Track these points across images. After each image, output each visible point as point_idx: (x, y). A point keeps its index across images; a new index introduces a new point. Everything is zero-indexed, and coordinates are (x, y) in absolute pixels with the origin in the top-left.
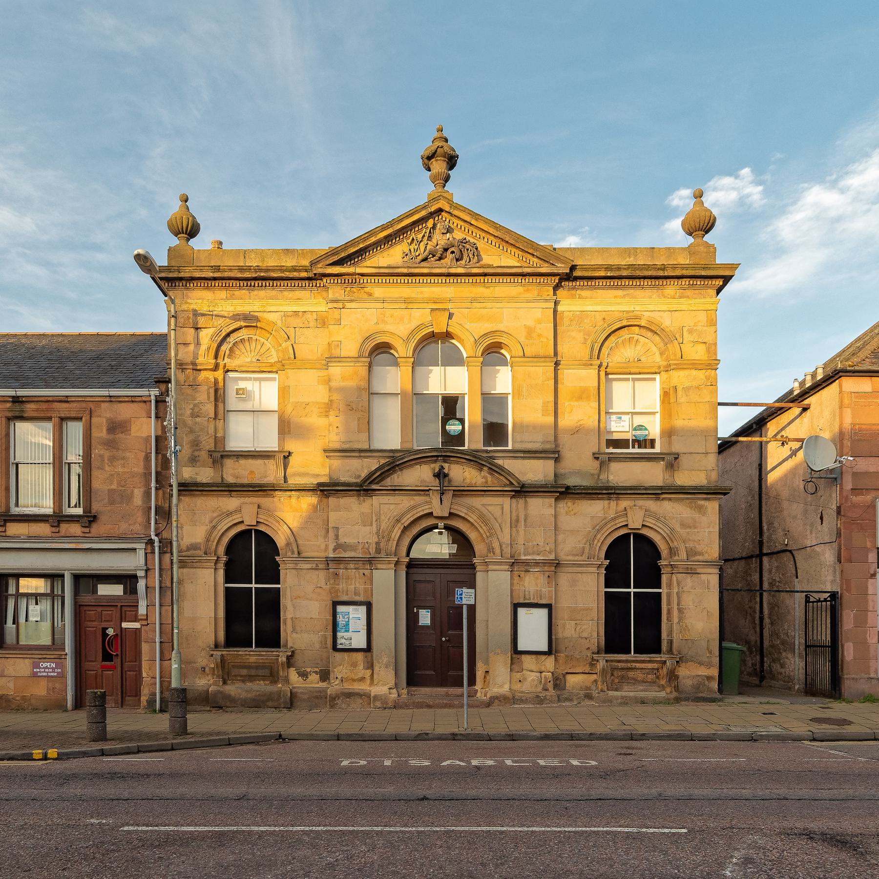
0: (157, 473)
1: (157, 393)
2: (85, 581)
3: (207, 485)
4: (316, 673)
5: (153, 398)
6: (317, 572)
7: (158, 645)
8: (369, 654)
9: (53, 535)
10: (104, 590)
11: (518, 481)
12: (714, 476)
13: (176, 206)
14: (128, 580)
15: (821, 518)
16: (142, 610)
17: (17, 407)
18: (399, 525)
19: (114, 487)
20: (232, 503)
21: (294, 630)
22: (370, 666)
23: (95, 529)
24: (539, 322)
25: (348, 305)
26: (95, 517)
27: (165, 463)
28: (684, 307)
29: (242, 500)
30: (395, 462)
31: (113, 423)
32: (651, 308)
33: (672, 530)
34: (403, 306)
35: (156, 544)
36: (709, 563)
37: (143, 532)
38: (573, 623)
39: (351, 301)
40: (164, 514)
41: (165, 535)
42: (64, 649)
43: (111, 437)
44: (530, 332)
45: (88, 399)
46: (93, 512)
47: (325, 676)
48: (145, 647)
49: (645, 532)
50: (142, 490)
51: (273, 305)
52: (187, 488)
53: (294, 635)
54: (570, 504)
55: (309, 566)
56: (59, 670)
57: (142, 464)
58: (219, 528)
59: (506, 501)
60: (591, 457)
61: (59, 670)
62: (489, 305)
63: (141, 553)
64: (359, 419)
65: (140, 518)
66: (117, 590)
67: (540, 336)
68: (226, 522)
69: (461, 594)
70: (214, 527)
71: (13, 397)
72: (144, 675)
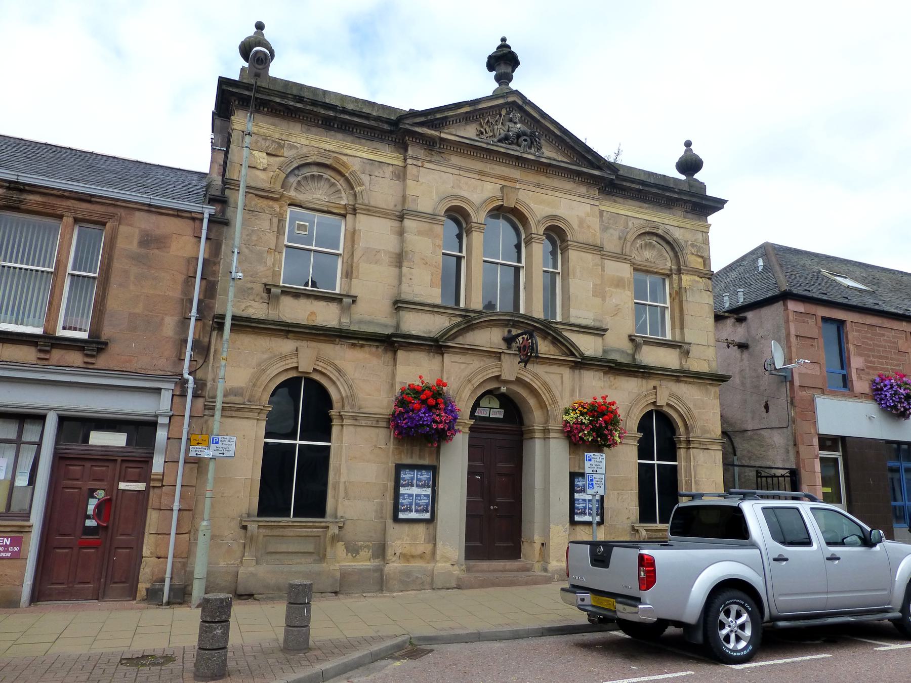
0: (199, 301)
1: (213, 212)
2: (75, 426)
3: (259, 321)
4: (367, 547)
5: (206, 216)
6: (377, 430)
7: (175, 513)
8: (431, 526)
9: (39, 362)
10: (98, 439)
11: (582, 354)
12: (714, 364)
13: (251, 31)
14: (141, 430)
15: (767, 407)
16: (158, 465)
17: (15, 195)
18: (470, 385)
19: (139, 310)
20: (287, 346)
21: (346, 496)
22: (433, 540)
23: (102, 361)
24: (588, 215)
25: (427, 165)
26: (106, 344)
27: (210, 290)
28: (688, 226)
29: (298, 344)
30: (470, 321)
31: (147, 235)
32: (666, 222)
33: (689, 409)
34: (478, 177)
35: (191, 385)
36: (714, 441)
37: (170, 368)
38: (616, 492)
39: (430, 162)
40: (203, 350)
41: (199, 374)
42: (27, 516)
43: (143, 251)
44: (581, 222)
45: (119, 203)
46: (103, 338)
47: (381, 551)
48: (153, 517)
49: (666, 409)
50: (176, 318)
51: (349, 148)
52: (243, 324)
53: (346, 502)
54: (612, 379)
55: (369, 423)
56: (17, 549)
57: (179, 287)
58: (268, 372)
59: (566, 372)
60: (627, 339)
61: (17, 549)
62: (549, 192)
63: (166, 396)
64: (432, 275)
65: (169, 351)
66: (118, 440)
67: (589, 227)
68: (279, 365)
69: (592, 480)
70: (264, 371)
71: (10, 182)
72: (146, 552)
